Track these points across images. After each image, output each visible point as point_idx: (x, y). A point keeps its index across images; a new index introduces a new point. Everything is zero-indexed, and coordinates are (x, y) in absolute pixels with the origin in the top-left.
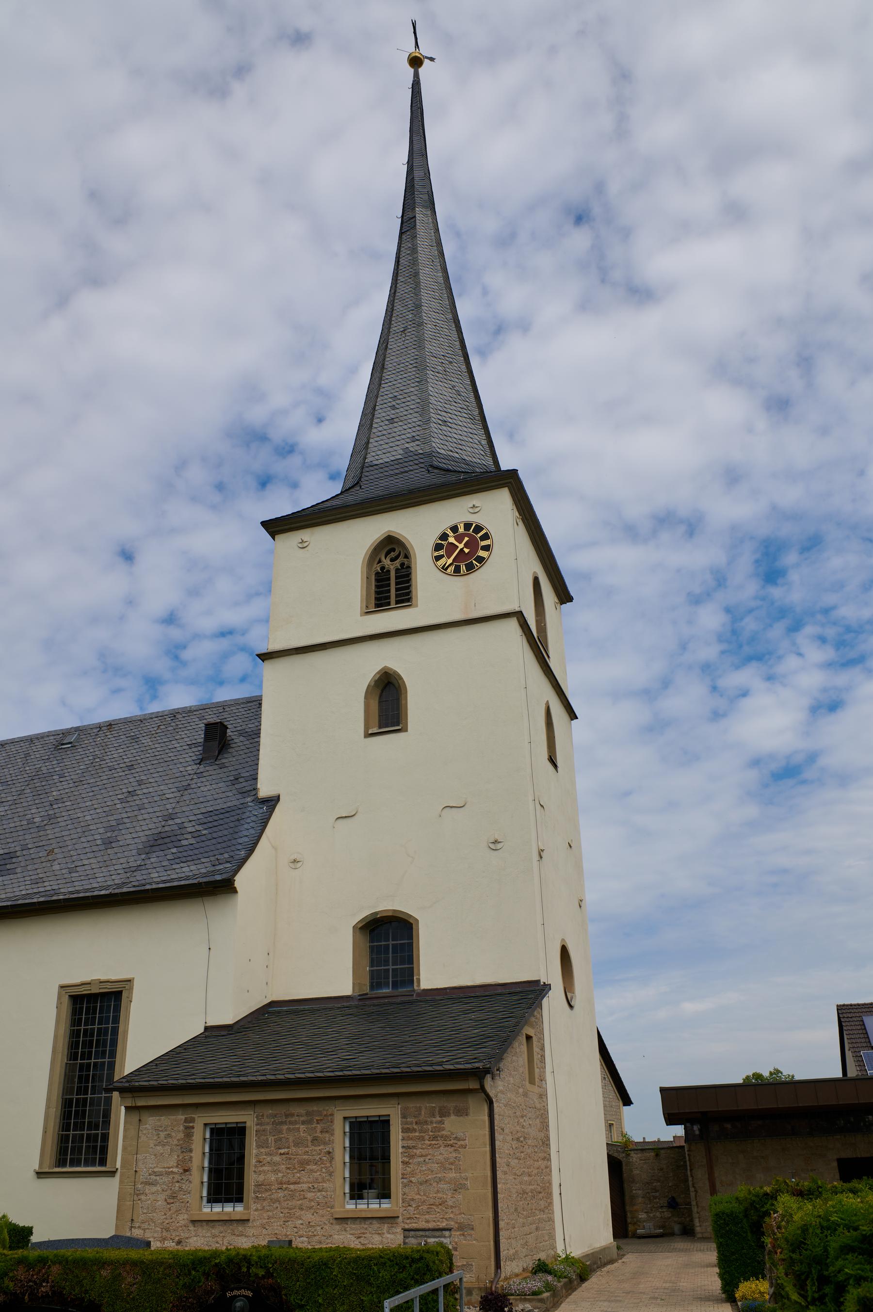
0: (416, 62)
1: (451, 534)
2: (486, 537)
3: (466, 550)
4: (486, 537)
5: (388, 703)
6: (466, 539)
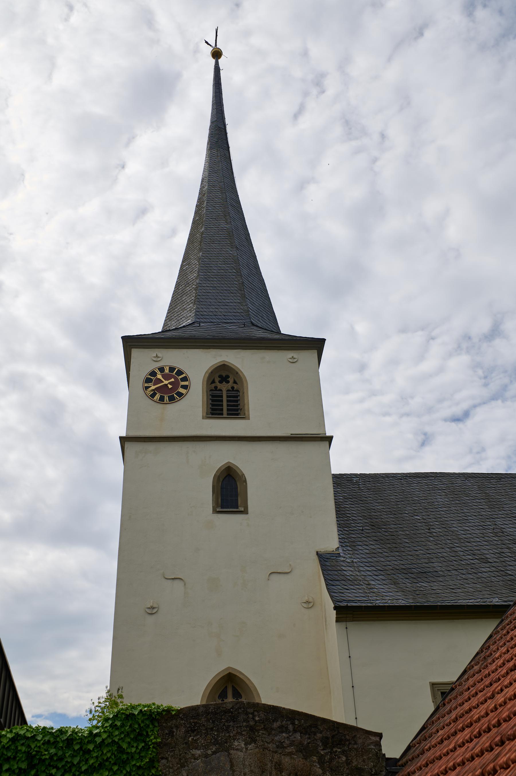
0: (217, 54)
1: (159, 373)
2: (185, 379)
3: (170, 386)
4: (185, 379)
5: (229, 492)
6: (173, 380)
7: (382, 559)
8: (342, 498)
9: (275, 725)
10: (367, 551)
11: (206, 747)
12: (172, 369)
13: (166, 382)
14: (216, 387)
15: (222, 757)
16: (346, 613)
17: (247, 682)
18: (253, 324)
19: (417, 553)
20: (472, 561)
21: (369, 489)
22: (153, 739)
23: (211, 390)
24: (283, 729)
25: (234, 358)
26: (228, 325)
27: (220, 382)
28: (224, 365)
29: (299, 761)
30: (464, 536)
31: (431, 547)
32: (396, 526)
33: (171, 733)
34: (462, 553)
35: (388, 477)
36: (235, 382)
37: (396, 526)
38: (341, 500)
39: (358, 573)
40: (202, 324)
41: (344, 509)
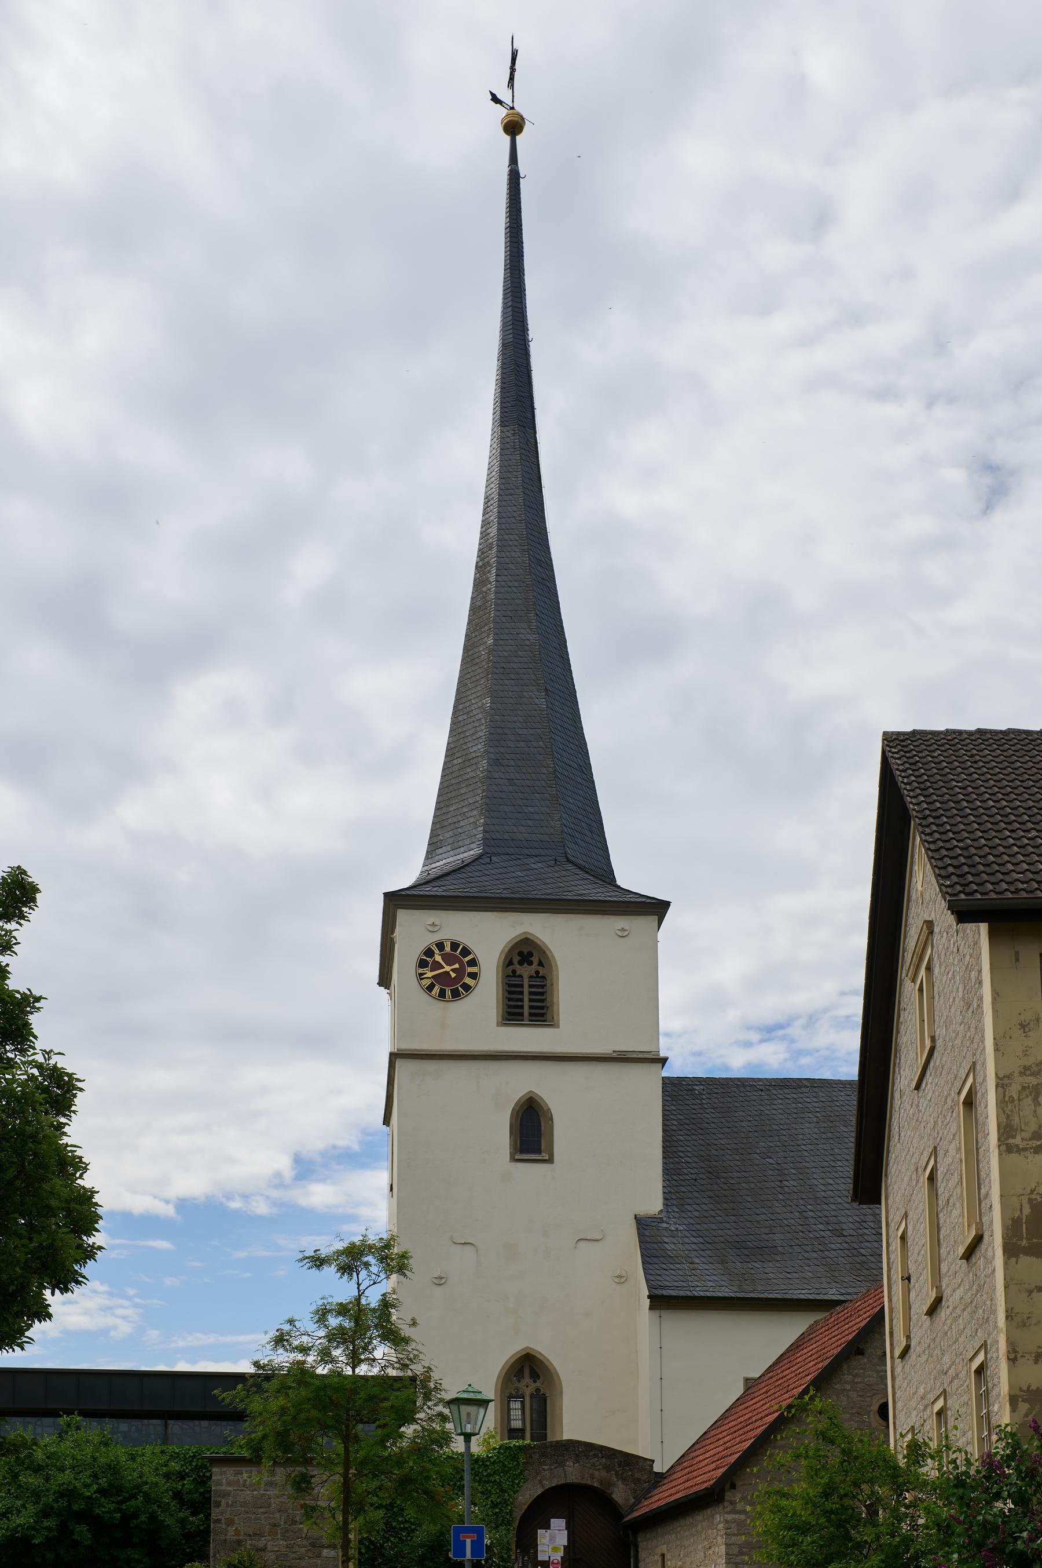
0: (513, 127)
1: (437, 951)
3: (453, 975)
5: (531, 1131)
6: (457, 966)
7: (714, 1227)
8: (675, 1123)
9: (591, 1453)
10: (697, 1214)
11: (551, 1465)
12: (455, 945)
13: (448, 968)
14: (514, 972)
15: (560, 1470)
16: (659, 1302)
17: (547, 1363)
18: (569, 861)
19: (759, 1218)
20: (822, 1233)
21: (714, 1108)
22: (522, 1460)
23: (508, 976)
24: (595, 1456)
25: (544, 928)
26: (532, 860)
27: (521, 963)
28: (527, 939)
29: (604, 1474)
30: (823, 1194)
31: (778, 1210)
32: (739, 1175)
33: (531, 1457)
34: (813, 1221)
35: (744, 1086)
36: (541, 964)
37: (739, 1175)
38: (674, 1128)
39: (681, 1246)
40: (494, 859)
41: (676, 1144)
